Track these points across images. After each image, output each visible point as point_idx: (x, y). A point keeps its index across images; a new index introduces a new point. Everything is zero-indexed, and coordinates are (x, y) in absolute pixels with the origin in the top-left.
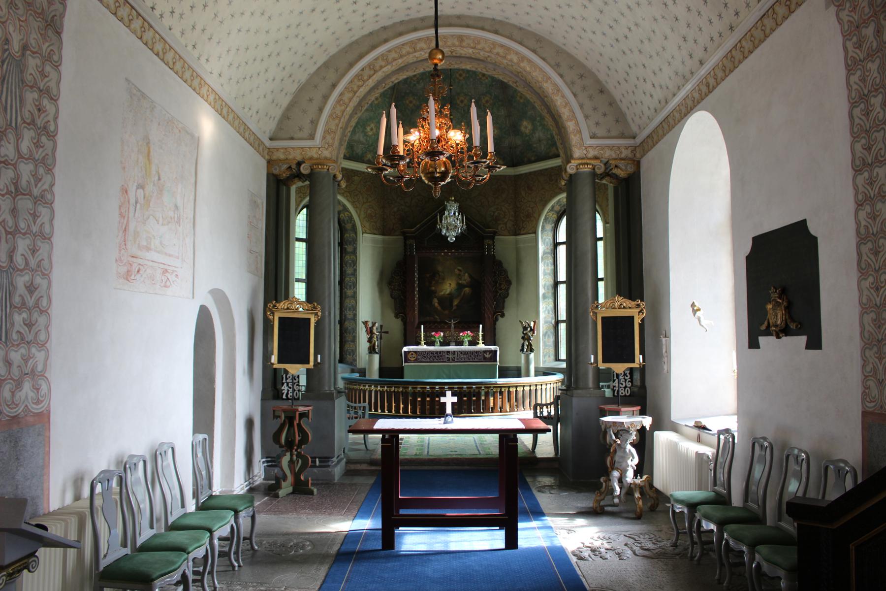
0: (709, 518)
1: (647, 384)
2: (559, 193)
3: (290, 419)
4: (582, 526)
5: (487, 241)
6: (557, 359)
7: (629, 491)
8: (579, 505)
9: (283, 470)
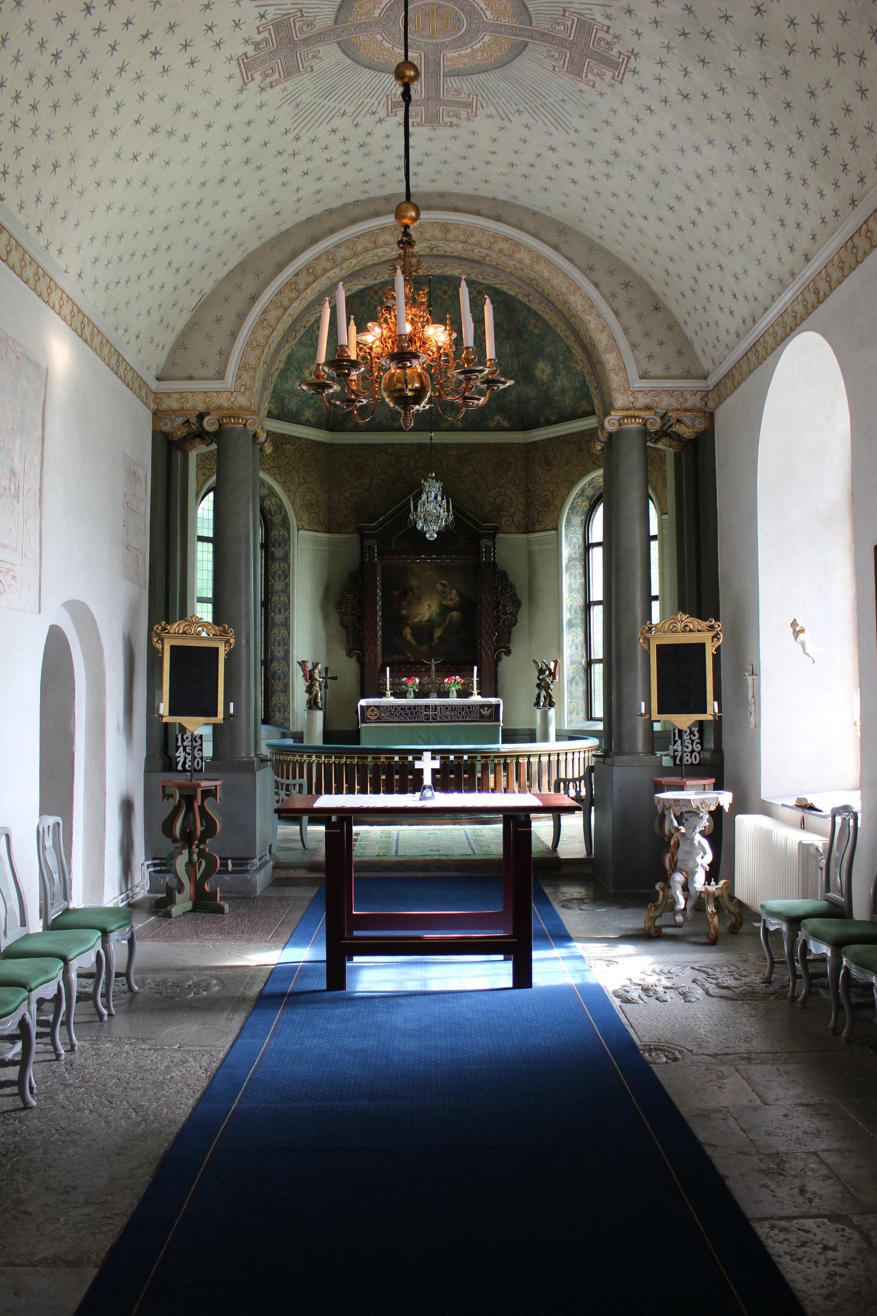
0: (818, 937)
1: (726, 747)
2: (593, 470)
3: (188, 799)
4: (628, 955)
5: (485, 542)
6: (589, 717)
7: (699, 904)
8: (624, 926)
9: (177, 877)
